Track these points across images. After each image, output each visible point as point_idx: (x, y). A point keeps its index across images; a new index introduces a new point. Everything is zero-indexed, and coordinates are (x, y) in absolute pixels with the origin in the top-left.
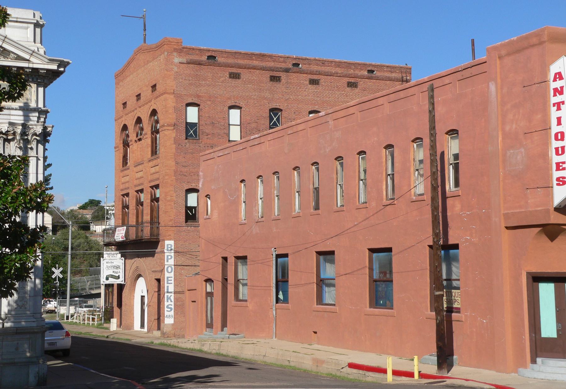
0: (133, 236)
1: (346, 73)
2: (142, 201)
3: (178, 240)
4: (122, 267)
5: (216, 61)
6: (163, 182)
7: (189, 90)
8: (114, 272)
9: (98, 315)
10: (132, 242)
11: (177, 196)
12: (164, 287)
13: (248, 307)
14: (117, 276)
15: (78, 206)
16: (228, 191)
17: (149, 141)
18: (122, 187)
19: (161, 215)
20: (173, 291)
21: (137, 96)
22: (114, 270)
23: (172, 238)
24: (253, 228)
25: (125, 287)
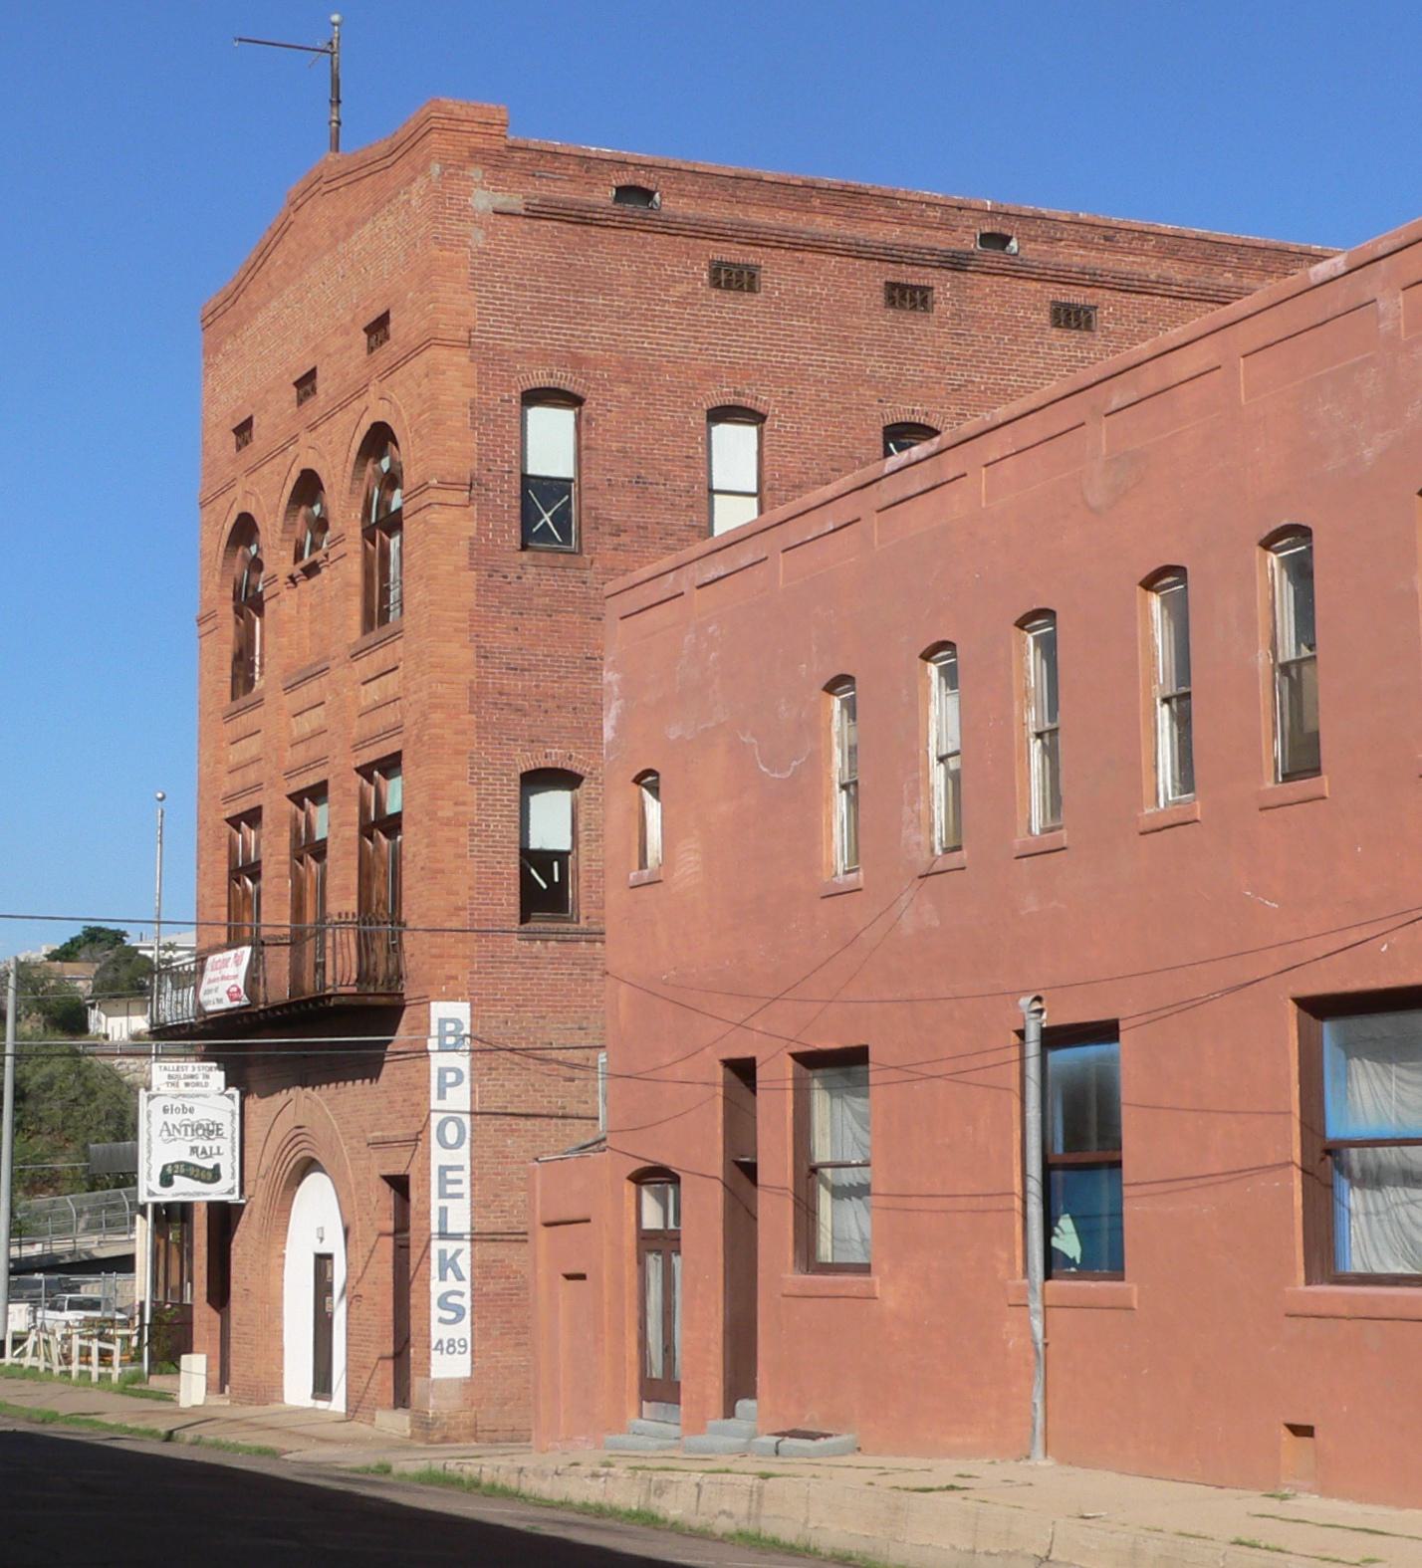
0: (278, 990)
1: (1203, 285)
2: (318, 838)
3: (488, 1000)
4: (230, 1128)
5: (652, 208)
6: (419, 738)
7: (536, 332)
8: (194, 1150)
9: (122, 1337)
10: (279, 1013)
11: (483, 803)
12: (429, 1212)
13: (876, 1298)
14: (207, 1170)
15: (45, 951)
16: (754, 741)
17: (353, 568)
18: (229, 784)
19: (410, 889)
20: (468, 1229)
21: (298, 384)
23: (460, 990)
24: (904, 905)
25: (244, 1218)
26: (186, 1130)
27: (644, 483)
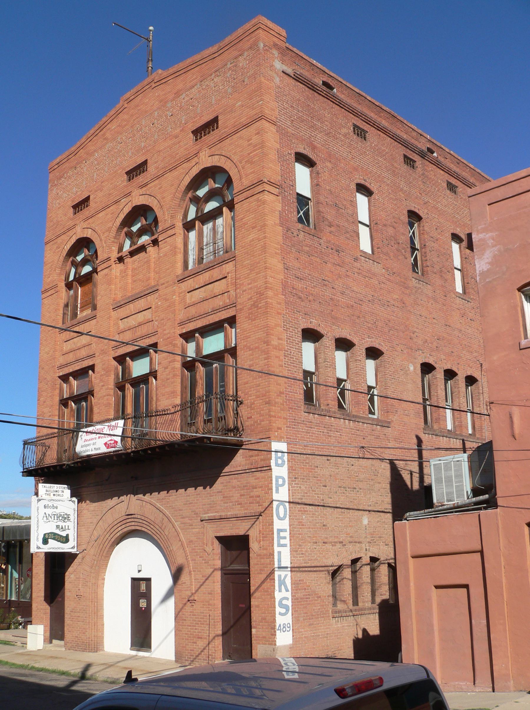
4: (73, 517)
22: (58, 524)
26: (54, 517)
27: (338, 207)
